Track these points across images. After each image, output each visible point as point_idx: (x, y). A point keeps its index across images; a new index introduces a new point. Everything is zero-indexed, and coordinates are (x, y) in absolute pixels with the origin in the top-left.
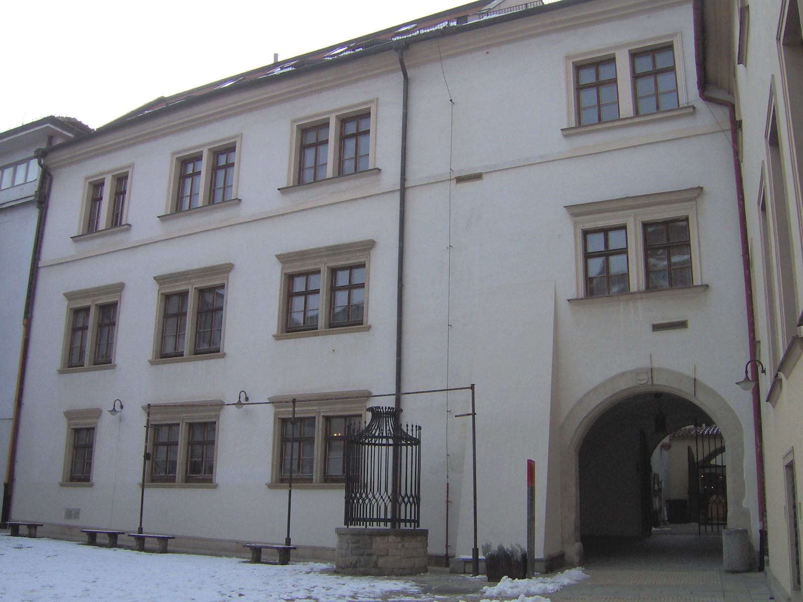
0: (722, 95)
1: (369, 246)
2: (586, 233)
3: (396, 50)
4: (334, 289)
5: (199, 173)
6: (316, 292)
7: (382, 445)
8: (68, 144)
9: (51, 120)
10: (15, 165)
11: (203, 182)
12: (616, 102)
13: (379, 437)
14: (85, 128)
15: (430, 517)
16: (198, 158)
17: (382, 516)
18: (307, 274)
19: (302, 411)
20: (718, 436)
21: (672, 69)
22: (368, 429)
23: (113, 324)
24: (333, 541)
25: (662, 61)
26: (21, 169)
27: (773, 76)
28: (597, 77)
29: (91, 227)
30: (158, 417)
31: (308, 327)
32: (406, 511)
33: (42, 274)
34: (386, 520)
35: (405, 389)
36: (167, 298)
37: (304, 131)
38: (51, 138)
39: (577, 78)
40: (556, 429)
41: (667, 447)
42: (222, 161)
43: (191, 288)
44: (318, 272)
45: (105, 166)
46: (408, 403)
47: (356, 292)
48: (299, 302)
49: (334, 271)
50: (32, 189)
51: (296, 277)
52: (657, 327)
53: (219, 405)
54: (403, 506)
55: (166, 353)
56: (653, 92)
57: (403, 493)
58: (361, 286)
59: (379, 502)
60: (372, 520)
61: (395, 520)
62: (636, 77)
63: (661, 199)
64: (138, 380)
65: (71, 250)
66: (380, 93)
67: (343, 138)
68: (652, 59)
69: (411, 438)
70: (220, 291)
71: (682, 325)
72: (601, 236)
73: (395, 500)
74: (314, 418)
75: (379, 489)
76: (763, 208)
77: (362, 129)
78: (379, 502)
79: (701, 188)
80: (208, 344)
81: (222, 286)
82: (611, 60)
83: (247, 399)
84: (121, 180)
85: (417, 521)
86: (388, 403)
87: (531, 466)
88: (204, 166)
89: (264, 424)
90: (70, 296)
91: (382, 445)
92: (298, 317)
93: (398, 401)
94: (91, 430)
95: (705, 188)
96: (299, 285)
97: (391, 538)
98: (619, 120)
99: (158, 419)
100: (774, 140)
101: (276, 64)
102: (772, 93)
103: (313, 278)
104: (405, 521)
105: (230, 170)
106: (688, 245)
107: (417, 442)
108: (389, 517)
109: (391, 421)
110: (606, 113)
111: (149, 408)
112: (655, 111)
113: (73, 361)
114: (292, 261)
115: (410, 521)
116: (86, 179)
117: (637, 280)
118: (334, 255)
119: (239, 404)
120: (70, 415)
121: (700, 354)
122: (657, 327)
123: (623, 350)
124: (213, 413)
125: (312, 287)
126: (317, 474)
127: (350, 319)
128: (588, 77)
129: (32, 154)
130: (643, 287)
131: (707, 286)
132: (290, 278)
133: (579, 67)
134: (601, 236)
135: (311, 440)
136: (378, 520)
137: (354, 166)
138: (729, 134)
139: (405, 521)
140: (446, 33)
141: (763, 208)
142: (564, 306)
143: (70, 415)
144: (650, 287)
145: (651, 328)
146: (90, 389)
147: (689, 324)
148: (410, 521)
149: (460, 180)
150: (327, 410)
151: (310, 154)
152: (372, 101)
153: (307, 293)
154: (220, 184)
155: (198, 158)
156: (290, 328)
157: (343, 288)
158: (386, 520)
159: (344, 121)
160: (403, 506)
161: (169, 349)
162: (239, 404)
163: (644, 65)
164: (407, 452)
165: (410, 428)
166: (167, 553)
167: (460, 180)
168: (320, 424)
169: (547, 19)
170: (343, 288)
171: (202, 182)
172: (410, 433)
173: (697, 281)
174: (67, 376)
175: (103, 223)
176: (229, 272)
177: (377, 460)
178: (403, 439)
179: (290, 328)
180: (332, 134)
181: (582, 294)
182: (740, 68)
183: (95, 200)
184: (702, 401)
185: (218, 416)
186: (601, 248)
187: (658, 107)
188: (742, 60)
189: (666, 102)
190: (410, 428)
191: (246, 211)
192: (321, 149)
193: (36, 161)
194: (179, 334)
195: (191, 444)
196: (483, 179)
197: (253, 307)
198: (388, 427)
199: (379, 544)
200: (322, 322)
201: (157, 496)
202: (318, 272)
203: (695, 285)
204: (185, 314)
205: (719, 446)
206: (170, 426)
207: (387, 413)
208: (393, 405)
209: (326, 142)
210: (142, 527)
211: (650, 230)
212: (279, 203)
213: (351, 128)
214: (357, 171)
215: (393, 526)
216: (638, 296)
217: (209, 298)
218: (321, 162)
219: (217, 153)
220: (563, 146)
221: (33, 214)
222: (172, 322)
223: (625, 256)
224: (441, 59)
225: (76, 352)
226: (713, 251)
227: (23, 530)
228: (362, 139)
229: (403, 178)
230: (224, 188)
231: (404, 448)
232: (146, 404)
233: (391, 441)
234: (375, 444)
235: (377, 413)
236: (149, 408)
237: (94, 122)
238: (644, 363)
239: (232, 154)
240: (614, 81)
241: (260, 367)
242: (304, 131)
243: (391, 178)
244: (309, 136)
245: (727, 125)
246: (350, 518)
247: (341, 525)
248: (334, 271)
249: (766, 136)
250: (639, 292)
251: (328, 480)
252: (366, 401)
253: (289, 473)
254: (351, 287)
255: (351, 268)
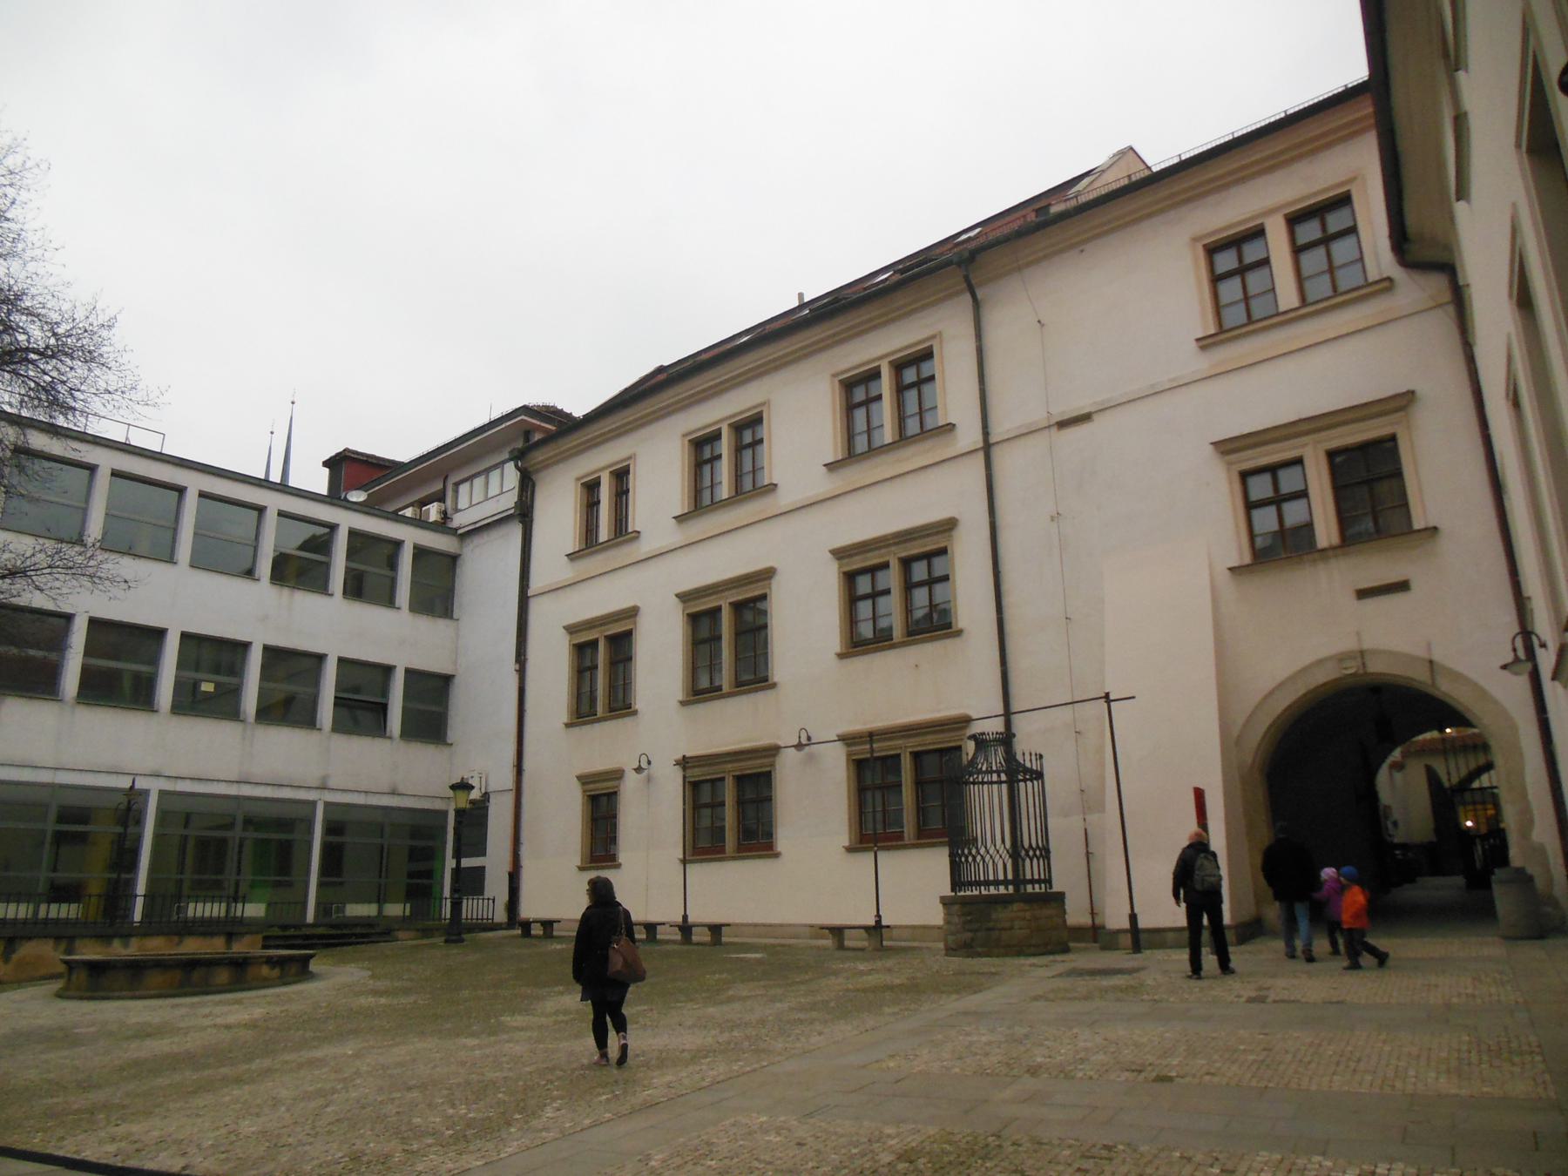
1: (949, 525)
2: (1245, 476)
3: (959, 264)
4: (909, 586)
5: (720, 456)
6: (887, 592)
7: (992, 783)
8: (550, 438)
9: (525, 410)
10: (487, 471)
11: (728, 467)
12: (1096, 1164)
13: (987, 772)
14: (569, 416)
15: (1066, 875)
16: (716, 436)
17: (1001, 877)
18: (872, 570)
19: (882, 748)
20: (1480, 746)
21: (1352, 230)
22: (973, 762)
23: (630, 659)
24: (936, 916)
26: (495, 476)
27: (1514, 205)
28: (1240, 259)
29: (589, 541)
30: (697, 771)
31: (881, 640)
32: (1032, 869)
33: (535, 607)
34: (1006, 882)
35: (1015, 707)
36: (694, 619)
37: (849, 385)
38: (527, 434)
39: (1211, 265)
40: (1230, 743)
41: (1398, 766)
42: (748, 437)
43: (724, 602)
44: (885, 566)
45: (599, 461)
46: (1021, 725)
47: (938, 588)
48: (864, 608)
49: (906, 563)
50: (509, 501)
51: (859, 573)
52: (1363, 594)
53: (773, 751)
54: (1028, 861)
55: (700, 691)
56: (1325, 267)
57: (1026, 845)
58: (945, 578)
59: (993, 860)
60: (987, 883)
61: (1018, 881)
62: (1297, 250)
63: (1350, 416)
64: (666, 727)
65: (567, 572)
66: (946, 327)
67: (900, 389)
68: (1321, 219)
69: (1031, 771)
70: (759, 605)
71: (1402, 586)
72: (1267, 478)
73: (1016, 853)
74: (898, 756)
75: (999, 842)
76: (1516, 404)
77: (925, 374)
78: (993, 860)
79: (1413, 392)
80: (754, 674)
81: (764, 597)
82: (1258, 233)
83: (809, 738)
84: (621, 475)
85: (1048, 881)
86: (995, 726)
87: (1199, 795)
88: (725, 446)
89: (835, 766)
90: (572, 630)
91: (992, 783)
92: (866, 630)
93: (1008, 724)
94: (612, 796)
95: (1419, 393)
96: (864, 584)
97: (1016, 906)
98: (1278, 314)
99: (696, 774)
100: (1524, 300)
101: (802, 306)
102: (1515, 231)
103: (880, 575)
104: (1032, 882)
105: (758, 448)
107: (1038, 775)
108: (1010, 877)
109: (1000, 750)
110: (1258, 309)
111: (685, 763)
113: (583, 712)
114: (850, 556)
115: (1039, 881)
116: (578, 479)
117: (1326, 532)
118: (905, 541)
119: (799, 746)
120: (584, 780)
121: (1441, 620)
122: (1363, 594)
123: (1322, 627)
124: (765, 761)
125: (881, 587)
126: (909, 829)
127: (935, 624)
128: (1227, 261)
129: (507, 456)
130: (1335, 539)
131: (1435, 528)
132: (850, 578)
133: (1212, 250)
134: (1267, 478)
135: (898, 786)
136: (997, 883)
137: (918, 429)
138: (1451, 309)
139: (1032, 882)
140: (1020, 234)
141: (1516, 404)
142: (1224, 577)
143: (584, 780)
144: (1350, 539)
145: (1354, 596)
146: (605, 746)
147: (1413, 585)
148: (1039, 881)
149: (1063, 424)
150: (915, 744)
151: (860, 414)
152: (933, 337)
153: (874, 595)
154: (747, 466)
155: (716, 436)
156: (856, 644)
157: (921, 584)
158: (1006, 882)
159: (899, 367)
160: (1028, 861)
161: (704, 683)
162: (799, 746)
164: (1026, 790)
165: (1027, 757)
167: (1063, 424)
168: (906, 764)
169: (1163, 191)
170: (921, 584)
171: (725, 469)
172: (1028, 765)
174: (576, 730)
175: (604, 534)
176: (770, 578)
177: (987, 804)
178: (1019, 773)
179: (856, 644)
180: (886, 385)
181: (1247, 559)
182: (1460, 208)
183: (591, 505)
184: (1446, 688)
185: (772, 765)
186: (1269, 493)
187: (1335, 288)
188: (1462, 193)
189: (1347, 279)
190: (1027, 757)
191: (786, 497)
192: (874, 406)
193: (512, 464)
194: (714, 667)
195: (741, 803)
197: (806, 619)
198: (997, 757)
199: (1001, 915)
200: (898, 633)
201: (706, 875)
202: (885, 566)
203: (1416, 526)
204: (719, 638)
205: (1482, 761)
206: (713, 781)
207: (995, 740)
208: (1001, 729)
209: (879, 397)
210: (1014, 730)
211: (1338, 459)
212: (823, 484)
213: (910, 375)
214: (925, 433)
215: (1017, 889)
216: (1331, 553)
217: (748, 616)
218: (875, 423)
219: (738, 428)
220: (1202, 363)
221: (515, 532)
222: (705, 648)
223: (1303, 502)
224: (1019, 269)
225: (585, 700)
226: (1440, 476)
227: (537, 930)
228: (926, 388)
229: (986, 433)
230: (754, 471)
231: (1022, 785)
232: (679, 756)
233: (1003, 777)
234: (983, 783)
235: (981, 742)
236: (685, 763)
237: (578, 408)
238: (1349, 644)
239: (758, 428)
240: (1265, 262)
241: (821, 696)
242: (849, 385)
243: (969, 436)
244: (856, 391)
245: (1447, 296)
246: (956, 883)
247: (948, 892)
248: (906, 563)
249: (1510, 295)
250: (1333, 548)
251: (925, 836)
252: (965, 728)
253: (874, 831)
254: (931, 582)
255: (928, 556)
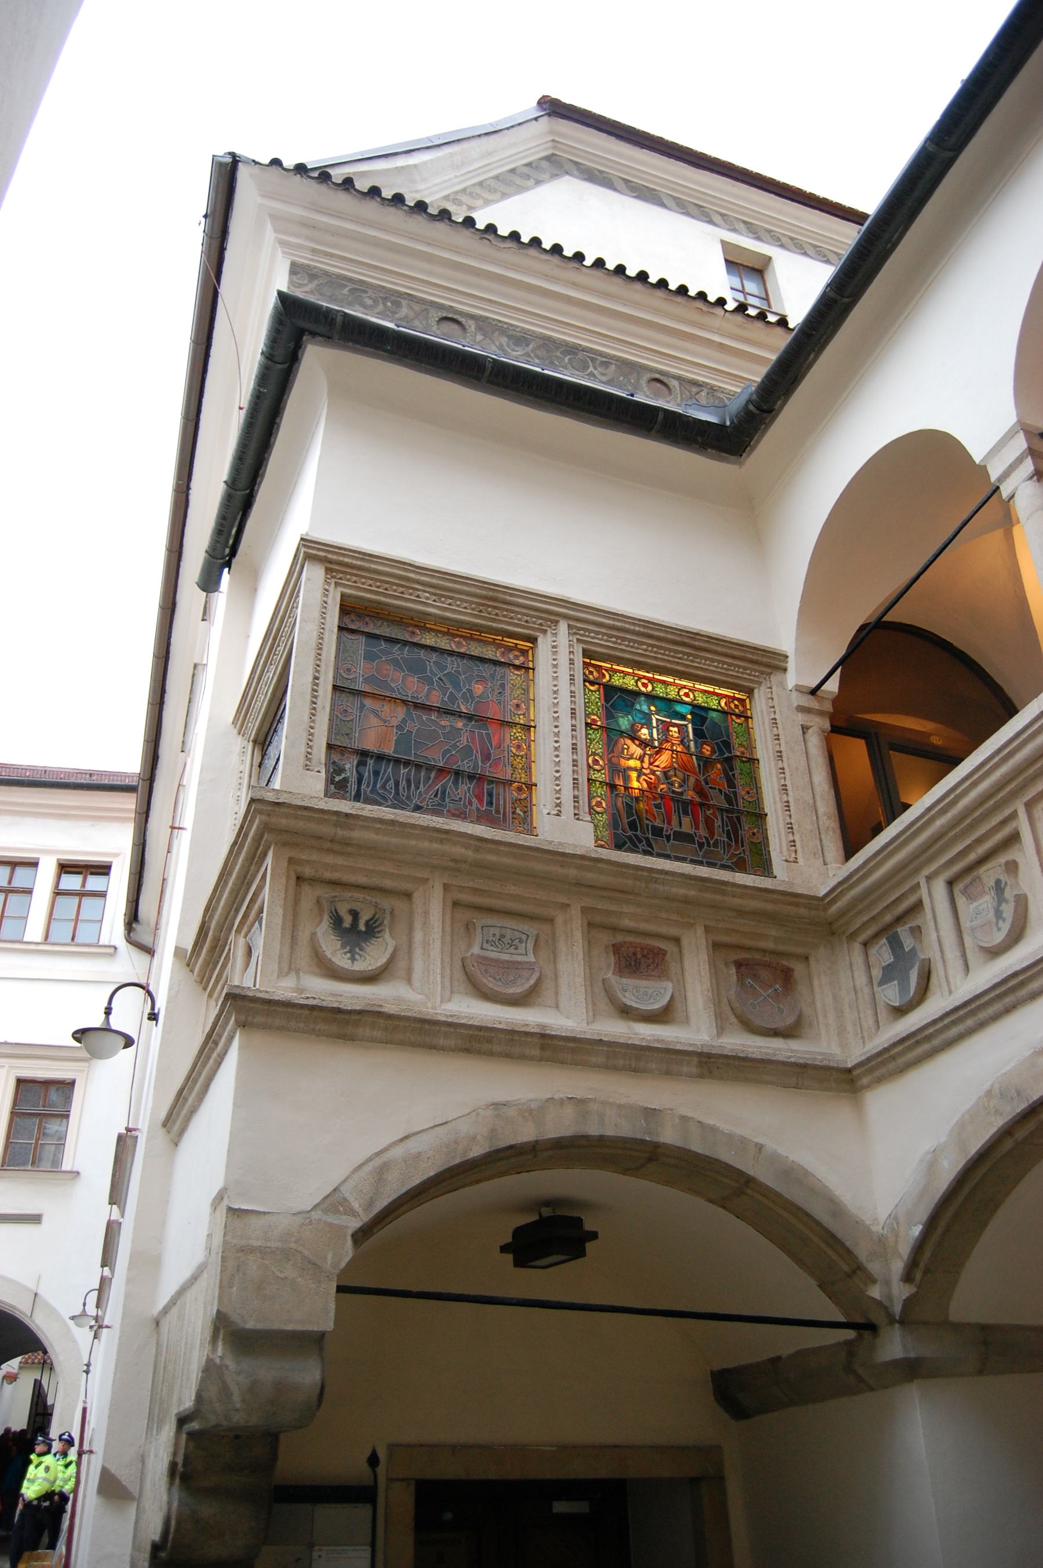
0: (147, 940)
25: (94, 883)
62: (58, 893)
71: (35, 1219)
98: (21, 942)
106: (66, 1116)
112: (69, 940)
147: (44, 1219)
163: (71, 882)
166: (963, 760)
173: (66, 1166)
187: (73, 939)
196: (740, 464)
